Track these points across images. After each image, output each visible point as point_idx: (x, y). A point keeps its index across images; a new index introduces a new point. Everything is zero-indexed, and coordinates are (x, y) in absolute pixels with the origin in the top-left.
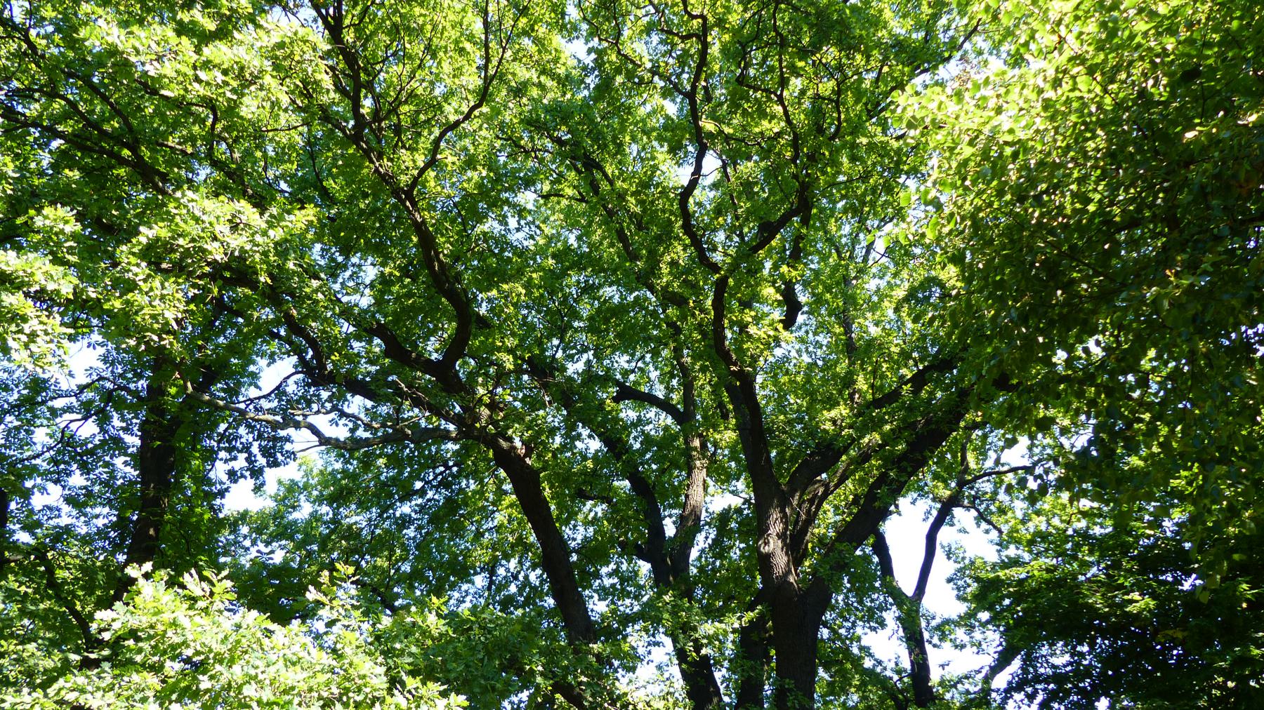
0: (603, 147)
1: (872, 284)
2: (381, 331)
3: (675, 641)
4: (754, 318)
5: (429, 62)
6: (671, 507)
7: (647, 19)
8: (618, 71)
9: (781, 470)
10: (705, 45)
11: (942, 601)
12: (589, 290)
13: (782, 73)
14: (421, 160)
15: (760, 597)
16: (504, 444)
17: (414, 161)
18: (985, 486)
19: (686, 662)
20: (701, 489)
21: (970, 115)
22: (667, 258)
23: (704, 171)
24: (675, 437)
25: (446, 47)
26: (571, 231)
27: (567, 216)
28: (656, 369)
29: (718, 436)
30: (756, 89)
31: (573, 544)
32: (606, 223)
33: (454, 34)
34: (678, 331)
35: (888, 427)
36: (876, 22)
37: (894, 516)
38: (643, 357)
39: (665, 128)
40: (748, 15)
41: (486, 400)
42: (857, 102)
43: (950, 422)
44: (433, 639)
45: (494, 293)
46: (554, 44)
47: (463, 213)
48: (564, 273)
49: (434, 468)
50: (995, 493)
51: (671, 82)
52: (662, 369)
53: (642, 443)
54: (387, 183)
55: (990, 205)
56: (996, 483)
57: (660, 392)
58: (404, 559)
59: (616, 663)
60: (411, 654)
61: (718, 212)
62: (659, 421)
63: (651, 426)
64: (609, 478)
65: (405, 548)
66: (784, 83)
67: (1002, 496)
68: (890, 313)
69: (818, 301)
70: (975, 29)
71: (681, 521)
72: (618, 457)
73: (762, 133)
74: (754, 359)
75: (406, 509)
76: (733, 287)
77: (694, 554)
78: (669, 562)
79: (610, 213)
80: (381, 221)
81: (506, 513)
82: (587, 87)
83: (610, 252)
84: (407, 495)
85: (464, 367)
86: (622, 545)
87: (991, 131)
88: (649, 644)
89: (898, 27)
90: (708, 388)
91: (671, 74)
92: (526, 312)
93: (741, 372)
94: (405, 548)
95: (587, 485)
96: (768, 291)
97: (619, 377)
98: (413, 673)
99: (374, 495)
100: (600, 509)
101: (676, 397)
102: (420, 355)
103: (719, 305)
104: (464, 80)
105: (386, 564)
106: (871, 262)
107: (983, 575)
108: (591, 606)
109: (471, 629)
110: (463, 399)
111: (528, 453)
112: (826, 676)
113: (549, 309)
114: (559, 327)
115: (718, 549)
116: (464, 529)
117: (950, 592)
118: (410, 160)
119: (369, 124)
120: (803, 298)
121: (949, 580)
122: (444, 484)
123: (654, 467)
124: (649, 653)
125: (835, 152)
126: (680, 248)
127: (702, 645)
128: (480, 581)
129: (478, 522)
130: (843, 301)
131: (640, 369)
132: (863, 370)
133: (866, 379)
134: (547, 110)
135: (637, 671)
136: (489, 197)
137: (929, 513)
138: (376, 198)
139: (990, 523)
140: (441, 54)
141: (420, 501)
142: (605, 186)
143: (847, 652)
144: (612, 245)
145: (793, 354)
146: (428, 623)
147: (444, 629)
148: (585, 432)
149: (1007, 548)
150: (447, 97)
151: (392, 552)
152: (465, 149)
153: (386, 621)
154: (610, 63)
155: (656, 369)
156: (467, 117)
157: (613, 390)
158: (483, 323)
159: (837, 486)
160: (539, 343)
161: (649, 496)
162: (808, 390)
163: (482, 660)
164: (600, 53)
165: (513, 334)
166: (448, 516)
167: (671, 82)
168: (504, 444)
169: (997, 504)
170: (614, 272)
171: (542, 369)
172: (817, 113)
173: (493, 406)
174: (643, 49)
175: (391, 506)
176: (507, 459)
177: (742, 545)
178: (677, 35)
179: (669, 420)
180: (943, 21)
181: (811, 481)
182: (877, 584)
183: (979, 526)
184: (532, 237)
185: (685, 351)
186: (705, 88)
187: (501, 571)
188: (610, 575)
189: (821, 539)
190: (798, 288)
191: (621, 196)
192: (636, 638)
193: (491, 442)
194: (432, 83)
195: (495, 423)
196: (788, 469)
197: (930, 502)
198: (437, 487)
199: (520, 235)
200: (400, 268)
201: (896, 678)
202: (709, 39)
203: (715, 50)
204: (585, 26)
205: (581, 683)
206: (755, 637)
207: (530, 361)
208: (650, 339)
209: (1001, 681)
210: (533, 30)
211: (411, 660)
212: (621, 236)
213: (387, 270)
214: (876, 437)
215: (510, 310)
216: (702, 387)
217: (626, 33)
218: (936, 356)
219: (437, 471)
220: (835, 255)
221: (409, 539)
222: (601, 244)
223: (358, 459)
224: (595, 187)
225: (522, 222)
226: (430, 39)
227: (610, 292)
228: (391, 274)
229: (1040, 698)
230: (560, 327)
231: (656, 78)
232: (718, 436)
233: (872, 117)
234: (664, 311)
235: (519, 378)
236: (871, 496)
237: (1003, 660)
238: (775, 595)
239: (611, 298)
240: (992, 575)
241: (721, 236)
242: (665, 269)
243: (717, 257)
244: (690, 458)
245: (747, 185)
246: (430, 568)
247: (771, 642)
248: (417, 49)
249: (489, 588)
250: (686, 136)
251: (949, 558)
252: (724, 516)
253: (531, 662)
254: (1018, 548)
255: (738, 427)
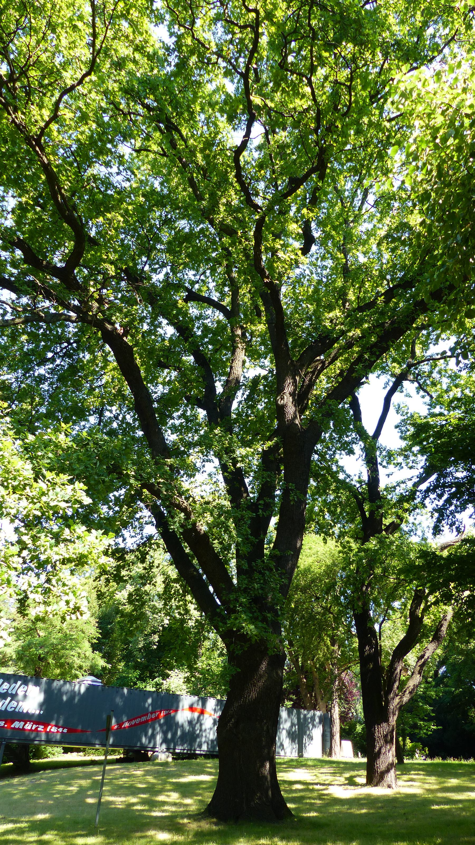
0: (180, 114)
1: (365, 227)
2: (20, 244)
3: (220, 459)
4: (282, 246)
5: (50, 35)
6: (221, 375)
7: (215, 11)
8: (192, 52)
9: (294, 353)
10: (257, 36)
11: (391, 439)
12: (167, 222)
13: (312, 63)
14: (46, 114)
15: (275, 433)
16: (109, 327)
17: (41, 116)
18: (425, 368)
19: (227, 472)
20: (240, 363)
21: (444, 92)
22: (224, 200)
23: (251, 136)
24: (224, 328)
25: (62, 24)
26: (156, 178)
27: (153, 167)
28: (213, 281)
29: (254, 328)
30: (293, 73)
31: (155, 396)
32: (182, 173)
33: (69, 14)
34: (229, 254)
35: (366, 325)
36: (382, 25)
37: (366, 385)
38: (204, 273)
39: (225, 102)
40: (289, 13)
41: (96, 296)
42: (364, 88)
43: (407, 323)
44: (63, 450)
45: (101, 219)
46: (145, 27)
47: (78, 159)
48: (150, 210)
49: (60, 344)
50: (431, 372)
51: (231, 64)
52: (217, 282)
53: (202, 331)
54: (22, 132)
55: (452, 158)
56: (431, 366)
57: (215, 296)
58: (41, 404)
59: (182, 472)
60: (49, 458)
61: (261, 166)
62: (214, 317)
63: (209, 320)
64: (179, 353)
65: (42, 398)
66: (313, 70)
67: (435, 375)
68: (375, 249)
69: (328, 236)
70: (453, 38)
71: (226, 384)
72: (186, 340)
73: (295, 108)
74: (281, 275)
75: (41, 371)
76: (268, 224)
77: (235, 405)
78: (218, 411)
79: (185, 165)
80: (18, 162)
81: (110, 374)
82: (169, 65)
83: (184, 194)
84: (43, 361)
85: (81, 273)
86: (188, 398)
87: (458, 106)
88: (204, 461)
89: (399, 30)
90: (248, 295)
91: (231, 58)
92: (123, 236)
93: (271, 283)
94: (42, 398)
95: (164, 358)
96: (294, 227)
97: (187, 285)
98: (51, 470)
99: (20, 361)
100: (174, 374)
101: (228, 300)
102: (49, 263)
103: (259, 237)
104: (78, 52)
105: (30, 407)
106: (363, 211)
107: (419, 421)
108: (166, 437)
109: (88, 444)
110: (80, 295)
111: (126, 333)
112: (315, 484)
113: (139, 235)
114: (147, 249)
115: (251, 401)
116: (81, 385)
117: (396, 434)
118: (38, 114)
119: (6, 83)
120: (316, 234)
121: (396, 427)
122: (68, 355)
123: (210, 347)
124: (204, 466)
125: (346, 127)
126: (232, 193)
127: (237, 462)
128: (93, 420)
129: (92, 381)
130: (343, 235)
131: (203, 281)
132: (353, 286)
133: (354, 293)
134: (141, 82)
135: (196, 477)
136: (95, 148)
137: (387, 383)
138: (14, 143)
139: (425, 391)
140: (59, 29)
141: (51, 366)
142: (181, 145)
143: (329, 469)
144: (185, 190)
145: (307, 272)
146: (60, 440)
147: (70, 444)
148: (165, 322)
149: (435, 407)
150: (66, 64)
151: (33, 400)
152: (79, 108)
153: (31, 438)
154: (187, 46)
155: (213, 281)
156: (80, 82)
157: (185, 294)
158: (93, 242)
159: (330, 363)
160: (133, 260)
161: (207, 367)
162: (314, 298)
163: (95, 464)
164: (179, 37)
165: (115, 251)
166: (71, 376)
167: (231, 64)
168: (109, 327)
169: (431, 379)
170: (186, 208)
171: (135, 277)
172: (335, 96)
173: (101, 301)
174: (211, 34)
175: (32, 369)
176: (112, 338)
177: (266, 400)
178: (237, 25)
179: (222, 317)
180: (430, 31)
181: (312, 360)
182: (351, 427)
183: (418, 393)
184: (128, 180)
185: (234, 269)
186: (255, 70)
187: (107, 414)
188: (179, 417)
189: (317, 397)
190: (313, 225)
191: (192, 152)
192: (195, 457)
193: (100, 325)
194: (54, 54)
195: (103, 312)
196: (299, 351)
197: (389, 377)
198: (63, 357)
199: (120, 178)
200: (34, 199)
201: (358, 485)
202: (260, 30)
203: (264, 40)
204: (168, 17)
205: (159, 483)
206: (271, 458)
207: (126, 271)
208: (209, 260)
209: (423, 487)
210: (128, 13)
211: (49, 461)
212: (192, 183)
213: (24, 199)
214: (358, 332)
215: (113, 232)
216: (244, 295)
217: (199, 22)
218: (401, 279)
219: (63, 346)
220: (340, 204)
221: (44, 391)
222: (177, 188)
223: (7, 336)
224: (173, 145)
225: (121, 168)
226: (50, 17)
227: (183, 224)
228: (27, 203)
229: (446, 496)
230: (147, 249)
231: (220, 60)
232: (254, 328)
233: (373, 103)
234: (220, 239)
235: (118, 283)
236: (351, 370)
237: (428, 471)
238: (286, 431)
239: (183, 228)
240: (425, 421)
241: (261, 186)
242: (222, 208)
243: (259, 201)
244: (234, 341)
245: (282, 147)
246: (59, 411)
247: (281, 461)
248: (41, 23)
249: (99, 424)
250: (242, 109)
251: (398, 412)
252: (256, 380)
253: (127, 469)
254: (441, 408)
255: (268, 321)
